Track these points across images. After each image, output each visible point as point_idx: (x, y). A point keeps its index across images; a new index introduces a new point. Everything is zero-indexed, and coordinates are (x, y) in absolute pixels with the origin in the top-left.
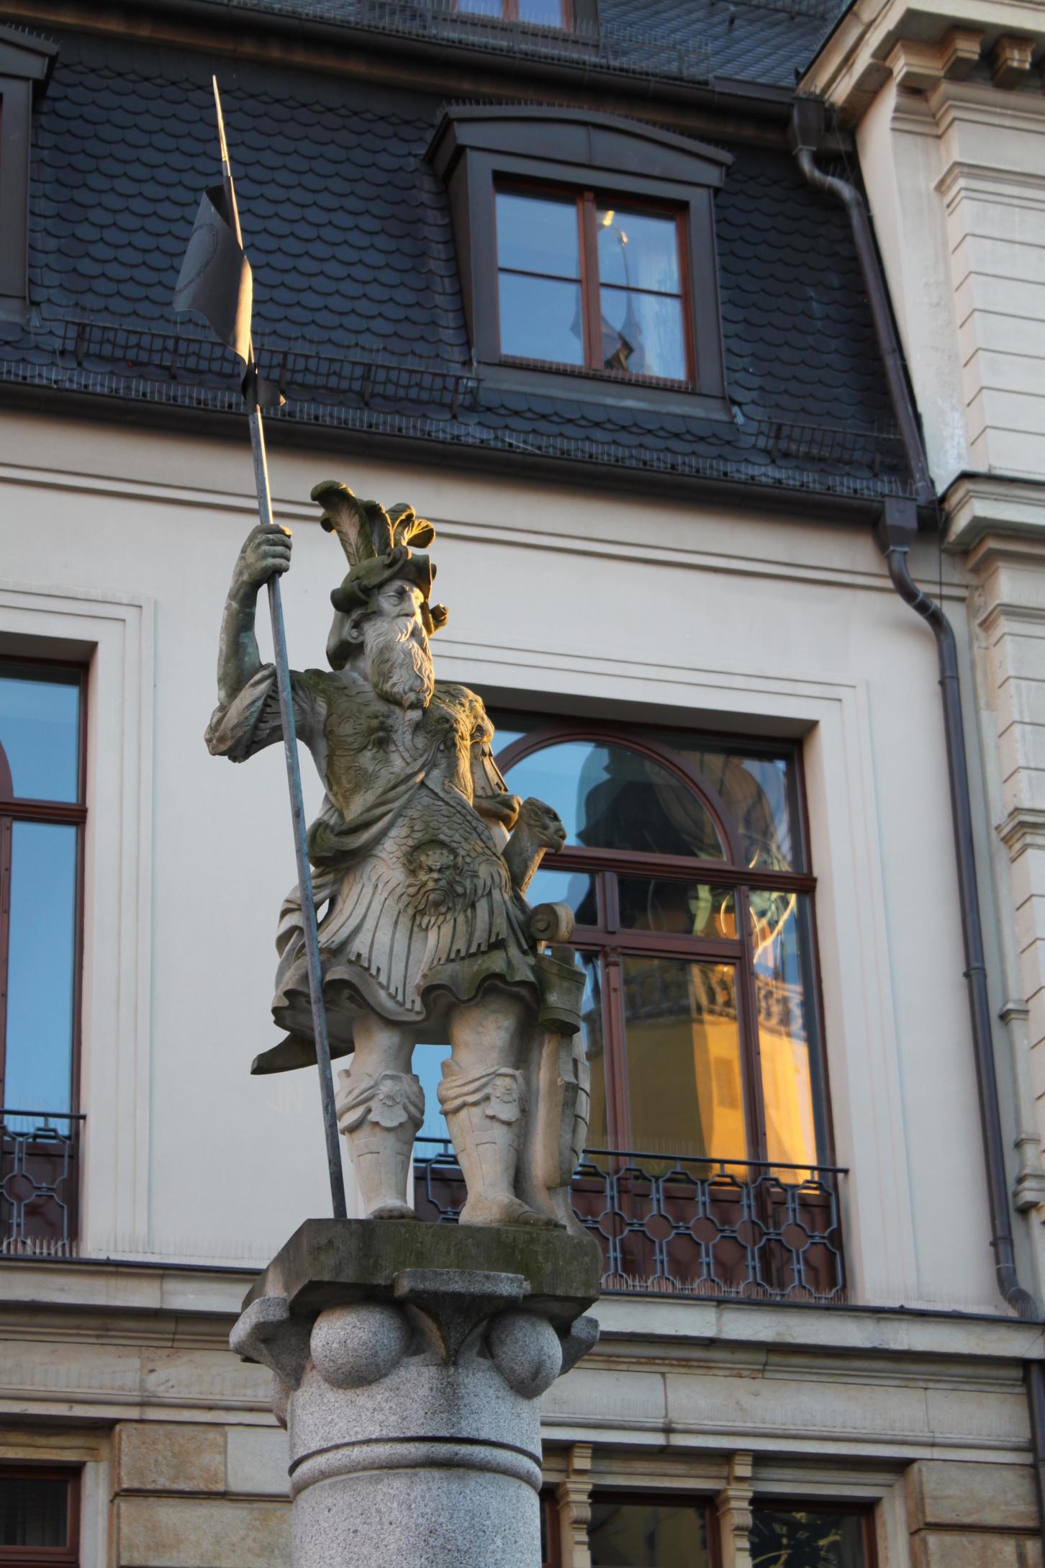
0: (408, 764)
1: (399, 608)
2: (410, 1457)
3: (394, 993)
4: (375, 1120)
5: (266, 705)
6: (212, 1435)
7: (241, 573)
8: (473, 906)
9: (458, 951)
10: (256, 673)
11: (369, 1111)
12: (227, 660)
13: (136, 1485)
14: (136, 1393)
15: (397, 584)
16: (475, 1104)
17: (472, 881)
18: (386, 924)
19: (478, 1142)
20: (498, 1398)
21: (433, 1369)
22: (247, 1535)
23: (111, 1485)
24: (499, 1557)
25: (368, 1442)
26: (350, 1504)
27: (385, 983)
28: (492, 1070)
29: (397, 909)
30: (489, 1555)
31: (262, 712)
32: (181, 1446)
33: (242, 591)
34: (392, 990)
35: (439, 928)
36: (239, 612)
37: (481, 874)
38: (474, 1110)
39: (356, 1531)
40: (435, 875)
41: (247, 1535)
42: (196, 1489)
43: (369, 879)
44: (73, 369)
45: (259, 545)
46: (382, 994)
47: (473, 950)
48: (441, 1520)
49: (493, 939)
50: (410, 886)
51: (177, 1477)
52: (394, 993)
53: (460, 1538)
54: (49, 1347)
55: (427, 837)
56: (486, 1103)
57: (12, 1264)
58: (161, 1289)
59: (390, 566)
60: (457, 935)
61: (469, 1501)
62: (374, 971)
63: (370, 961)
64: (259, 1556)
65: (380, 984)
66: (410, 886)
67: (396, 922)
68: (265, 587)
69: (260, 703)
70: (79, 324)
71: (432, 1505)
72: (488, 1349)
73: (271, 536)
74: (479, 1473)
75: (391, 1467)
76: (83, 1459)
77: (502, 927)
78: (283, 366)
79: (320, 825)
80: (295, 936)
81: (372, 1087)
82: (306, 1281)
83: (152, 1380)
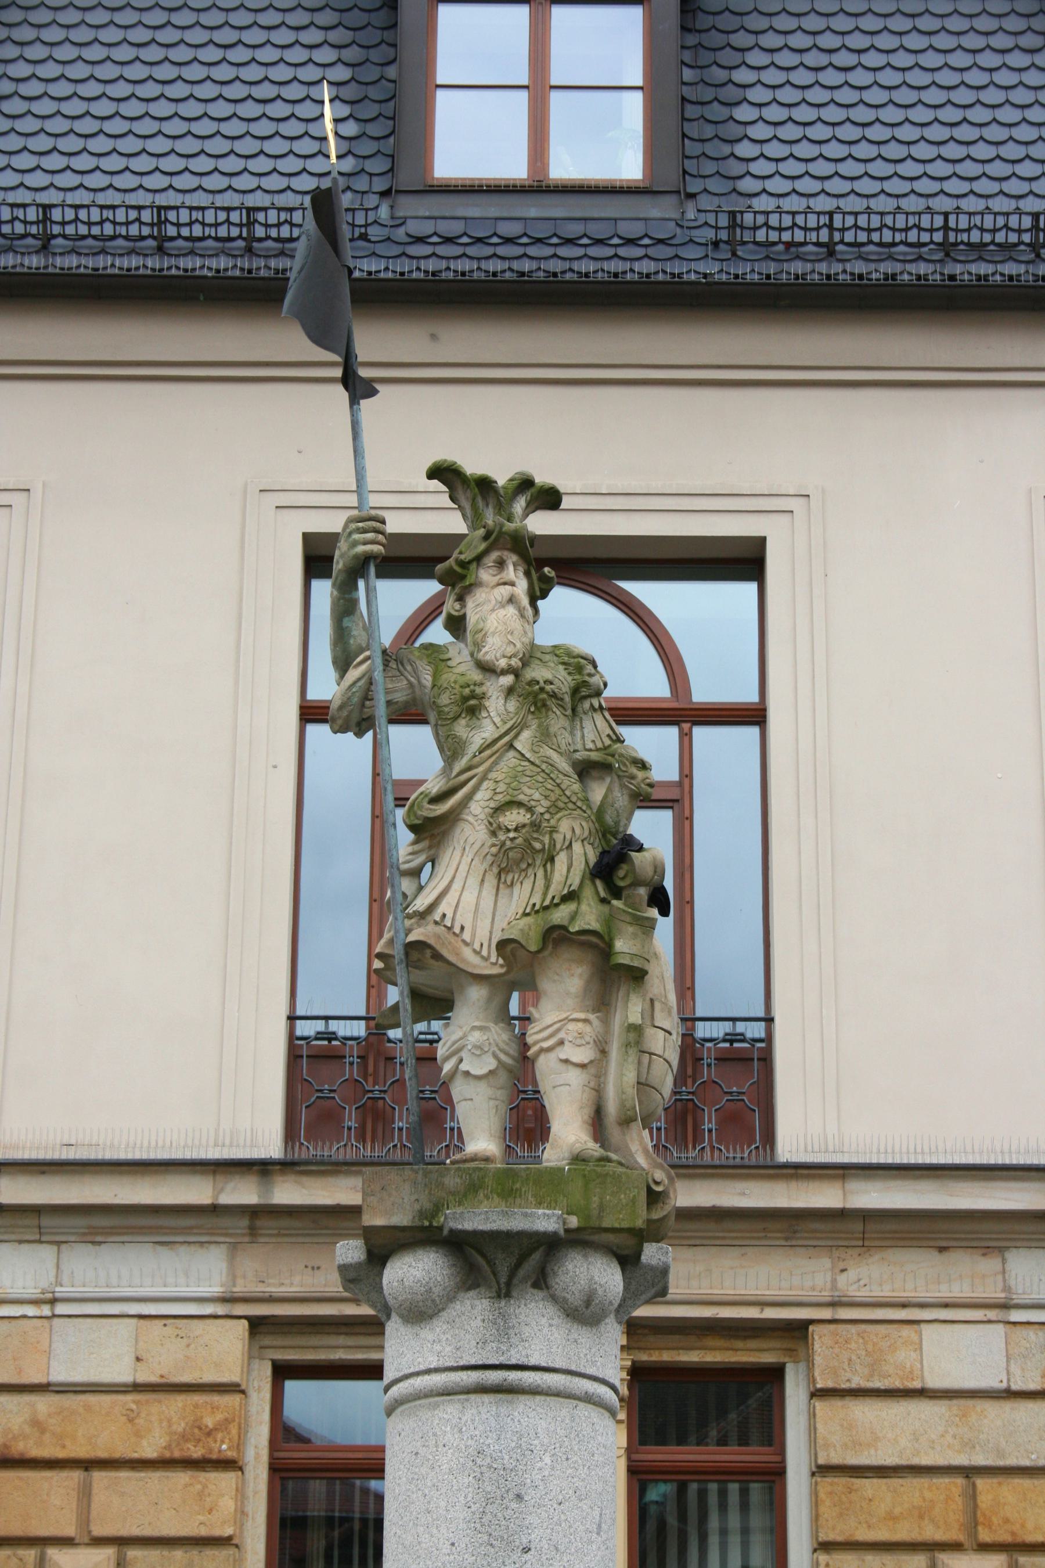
1: (498, 577)
2: (462, 1384)
6: (906, 1331)
8: (552, 859)
9: (534, 905)
11: (461, 1060)
13: (830, 1384)
14: (826, 1294)
15: (494, 555)
17: (551, 837)
18: (473, 882)
20: (551, 1325)
21: (486, 1302)
22: (946, 1432)
24: (546, 1473)
25: (428, 1371)
26: (414, 1429)
27: (468, 940)
28: (564, 1016)
29: (483, 869)
30: (536, 1471)
32: (874, 1344)
34: (477, 946)
36: (339, 599)
37: (561, 829)
39: (417, 1454)
40: (512, 835)
41: (946, 1432)
42: (892, 1386)
43: (459, 842)
44: (729, 259)
47: (547, 903)
48: (490, 1441)
50: (494, 845)
51: (872, 1376)
52: (478, 949)
53: (507, 1457)
54: (736, 1252)
55: (508, 798)
57: (691, 1171)
60: (535, 889)
61: (517, 1423)
62: (457, 930)
63: (453, 919)
64: (959, 1452)
66: (494, 845)
67: (483, 881)
70: (729, 212)
71: (481, 1428)
72: (541, 1281)
73: (360, 525)
74: (527, 1397)
75: (449, 1394)
76: (782, 1360)
78: (946, 228)
81: (461, 1039)
83: (842, 1280)
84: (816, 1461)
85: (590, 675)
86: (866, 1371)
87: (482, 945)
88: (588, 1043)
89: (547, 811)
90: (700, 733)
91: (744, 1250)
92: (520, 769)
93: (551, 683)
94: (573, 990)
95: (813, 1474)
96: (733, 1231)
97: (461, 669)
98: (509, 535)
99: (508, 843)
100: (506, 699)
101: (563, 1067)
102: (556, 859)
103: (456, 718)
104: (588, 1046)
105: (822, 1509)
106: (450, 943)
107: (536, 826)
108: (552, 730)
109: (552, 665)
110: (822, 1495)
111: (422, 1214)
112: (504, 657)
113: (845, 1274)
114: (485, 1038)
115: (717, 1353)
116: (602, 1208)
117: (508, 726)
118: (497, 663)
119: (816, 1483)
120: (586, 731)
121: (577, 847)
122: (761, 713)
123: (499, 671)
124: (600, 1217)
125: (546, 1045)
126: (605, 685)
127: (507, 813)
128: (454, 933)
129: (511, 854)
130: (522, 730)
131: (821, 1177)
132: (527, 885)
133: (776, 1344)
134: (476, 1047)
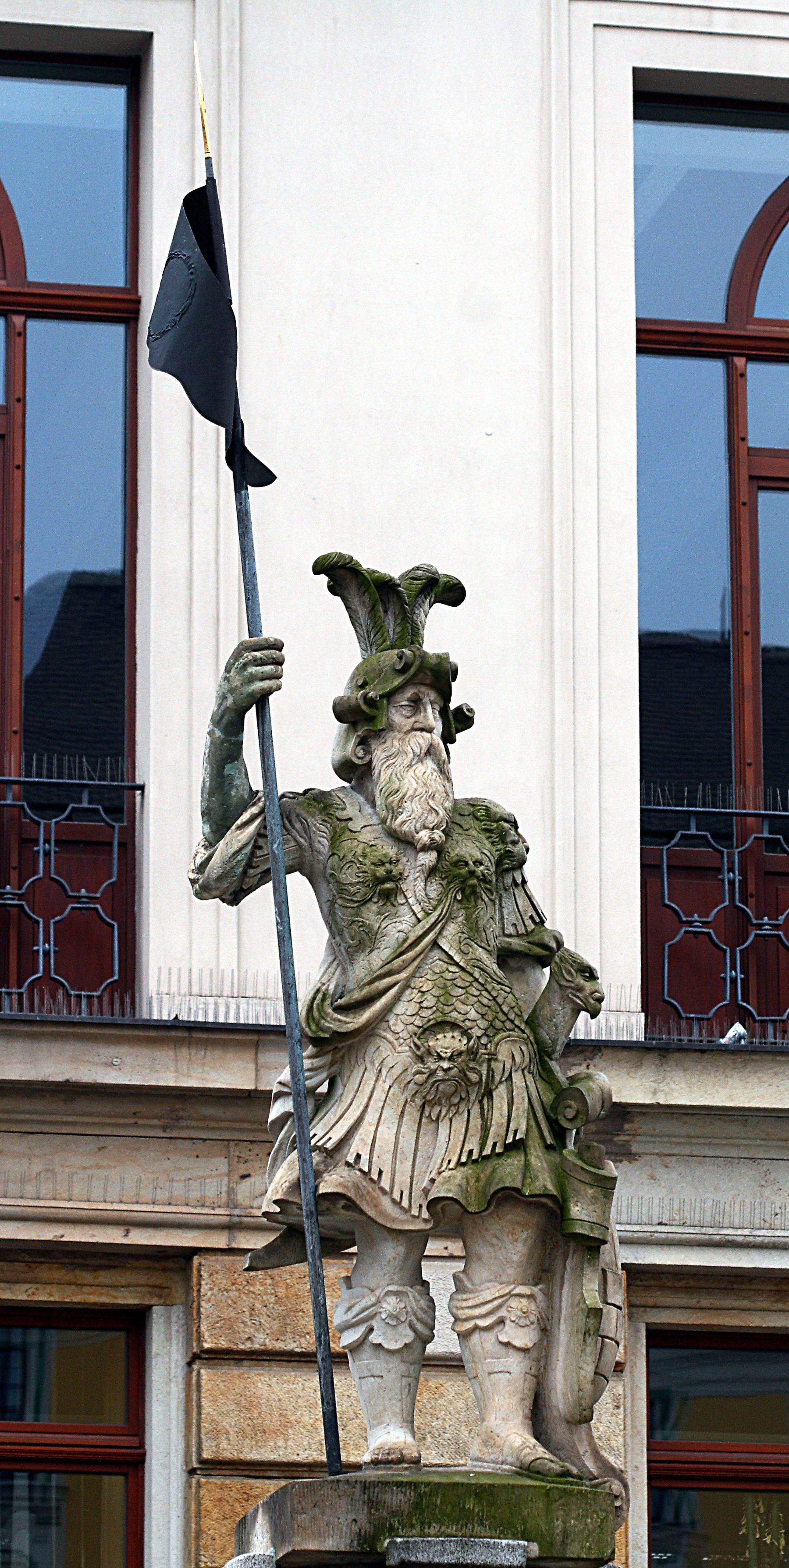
0: (419, 921)
1: (413, 719)
3: (398, 1199)
4: (376, 1341)
5: (256, 847)
7: (224, 697)
8: (489, 1094)
9: (471, 1152)
10: (245, 809)
11: (371, 1330)
12: (211, 794)
13: (223, 1344)
15: (409, 693)
16: (487, 1329)
17: (489, 1066)
18: (391, 1114)
19: (490, 1370)
23: (188, 1342)
27: (387, 1188)
29: (402, 1099)
31: (252, 854)
32: (288, 1287)
33: (226, 718)
35: (451, 1120)
36: (222, 742)
37: (500, 1057)
38: (485, 1335)
40: (446, 1065)
43: (372, 1062)
45: (245, 666)
46: (385, 1201)
47: (487, 1151)
49: (510, 1140)
50: (419, 1072)
56: (501, 1327)
58: (256, 1059)
59: (402, 671)
60: (470, 1131)
65: (382, 1190)
66: (419, 1072)
67: (402, 1113)
68: (253, 710)
69: (247, 850)
73: (258, 654)
76: (147, 1302)
77: (521, 1124)
79: (320, 996)
80: (289, 1123)
81: (373, 1305)
82: (290, 1549)
84: (199, 1454)
85: (514, 843)
86: (276, 1325)
87: (402, 1193)
88: (532, 1323)
89: (485, 1034)
90: (36, 329)
91: (103, 1141)
92: (449, 976)
93: (481, 864)
94: (516, 1258)
95: (192, 1472)
96: (90, 1115)
97: (367, 836)
98: (431, 670)
99: (440, 1074)
100: (426, 880)
101: (502, 1350)
102: (495, 1094)
103: (364, 902)
104: (532, 1327)
105: (206, 1522)
106: (368, 1193)
107: (472, 1053)
108: (481, 923)
109: (474, 833)
110: (207, 1503)
111: (361, 1537)
112: (425, 827)
113: (247, 1182)
114: (403, 1305)
115: (54, 1289)
116: (565, 1534)
117: (432, 919)
118: (418, 836)
119: (199, 1485)
120: (505, 911)
121: (517, 1078)
122: (131, 306)
123: (419, 846)
124: (564, 1544)
125: (482, 1323)
126: (527, 850)
127: (440, 1036)
128: (371, 1180)
129: (441, 1087)
130: (446, 923)
131: (224, 1045)
132: (459, 1124)
133: (141, 1278)
134: (391, 1316)
